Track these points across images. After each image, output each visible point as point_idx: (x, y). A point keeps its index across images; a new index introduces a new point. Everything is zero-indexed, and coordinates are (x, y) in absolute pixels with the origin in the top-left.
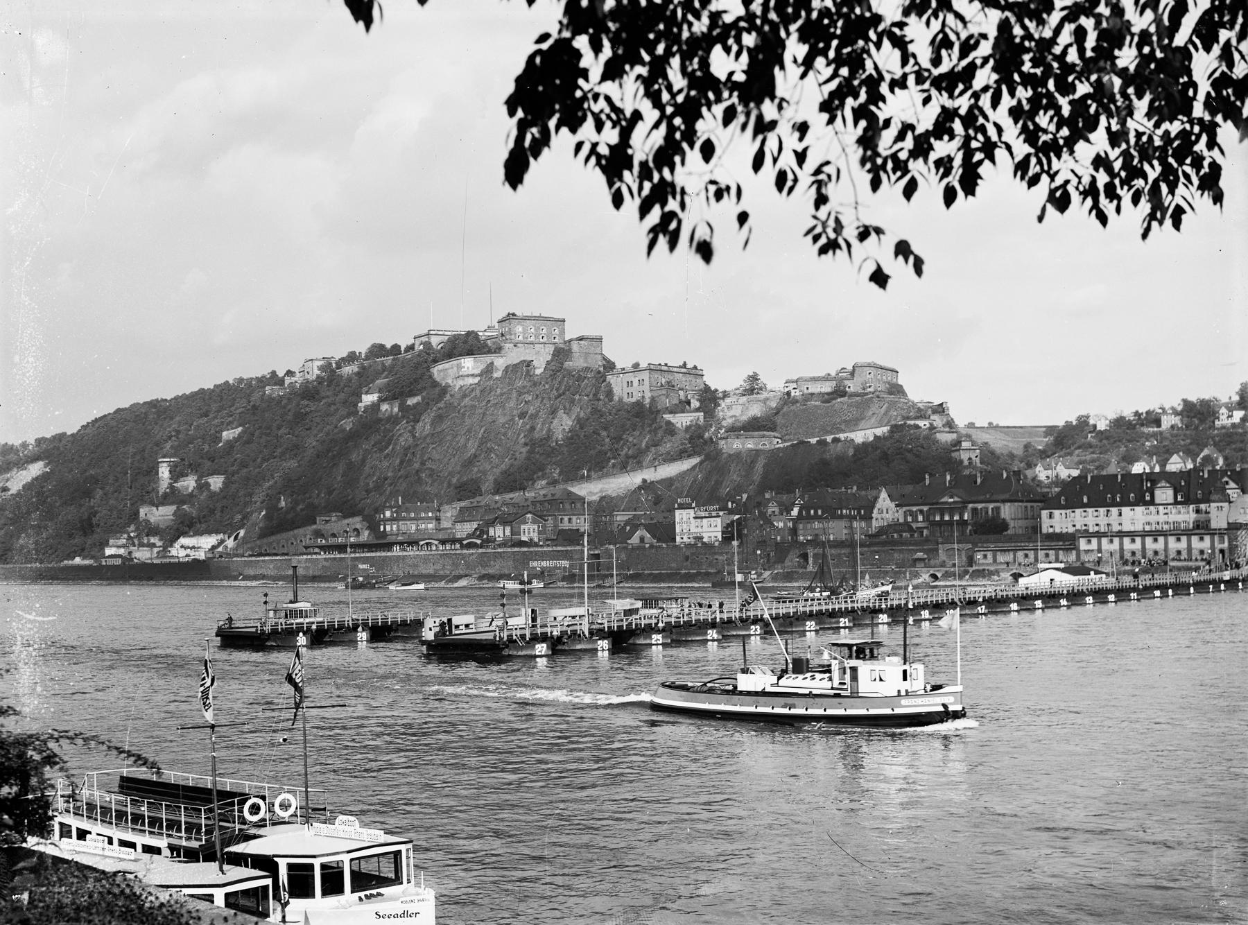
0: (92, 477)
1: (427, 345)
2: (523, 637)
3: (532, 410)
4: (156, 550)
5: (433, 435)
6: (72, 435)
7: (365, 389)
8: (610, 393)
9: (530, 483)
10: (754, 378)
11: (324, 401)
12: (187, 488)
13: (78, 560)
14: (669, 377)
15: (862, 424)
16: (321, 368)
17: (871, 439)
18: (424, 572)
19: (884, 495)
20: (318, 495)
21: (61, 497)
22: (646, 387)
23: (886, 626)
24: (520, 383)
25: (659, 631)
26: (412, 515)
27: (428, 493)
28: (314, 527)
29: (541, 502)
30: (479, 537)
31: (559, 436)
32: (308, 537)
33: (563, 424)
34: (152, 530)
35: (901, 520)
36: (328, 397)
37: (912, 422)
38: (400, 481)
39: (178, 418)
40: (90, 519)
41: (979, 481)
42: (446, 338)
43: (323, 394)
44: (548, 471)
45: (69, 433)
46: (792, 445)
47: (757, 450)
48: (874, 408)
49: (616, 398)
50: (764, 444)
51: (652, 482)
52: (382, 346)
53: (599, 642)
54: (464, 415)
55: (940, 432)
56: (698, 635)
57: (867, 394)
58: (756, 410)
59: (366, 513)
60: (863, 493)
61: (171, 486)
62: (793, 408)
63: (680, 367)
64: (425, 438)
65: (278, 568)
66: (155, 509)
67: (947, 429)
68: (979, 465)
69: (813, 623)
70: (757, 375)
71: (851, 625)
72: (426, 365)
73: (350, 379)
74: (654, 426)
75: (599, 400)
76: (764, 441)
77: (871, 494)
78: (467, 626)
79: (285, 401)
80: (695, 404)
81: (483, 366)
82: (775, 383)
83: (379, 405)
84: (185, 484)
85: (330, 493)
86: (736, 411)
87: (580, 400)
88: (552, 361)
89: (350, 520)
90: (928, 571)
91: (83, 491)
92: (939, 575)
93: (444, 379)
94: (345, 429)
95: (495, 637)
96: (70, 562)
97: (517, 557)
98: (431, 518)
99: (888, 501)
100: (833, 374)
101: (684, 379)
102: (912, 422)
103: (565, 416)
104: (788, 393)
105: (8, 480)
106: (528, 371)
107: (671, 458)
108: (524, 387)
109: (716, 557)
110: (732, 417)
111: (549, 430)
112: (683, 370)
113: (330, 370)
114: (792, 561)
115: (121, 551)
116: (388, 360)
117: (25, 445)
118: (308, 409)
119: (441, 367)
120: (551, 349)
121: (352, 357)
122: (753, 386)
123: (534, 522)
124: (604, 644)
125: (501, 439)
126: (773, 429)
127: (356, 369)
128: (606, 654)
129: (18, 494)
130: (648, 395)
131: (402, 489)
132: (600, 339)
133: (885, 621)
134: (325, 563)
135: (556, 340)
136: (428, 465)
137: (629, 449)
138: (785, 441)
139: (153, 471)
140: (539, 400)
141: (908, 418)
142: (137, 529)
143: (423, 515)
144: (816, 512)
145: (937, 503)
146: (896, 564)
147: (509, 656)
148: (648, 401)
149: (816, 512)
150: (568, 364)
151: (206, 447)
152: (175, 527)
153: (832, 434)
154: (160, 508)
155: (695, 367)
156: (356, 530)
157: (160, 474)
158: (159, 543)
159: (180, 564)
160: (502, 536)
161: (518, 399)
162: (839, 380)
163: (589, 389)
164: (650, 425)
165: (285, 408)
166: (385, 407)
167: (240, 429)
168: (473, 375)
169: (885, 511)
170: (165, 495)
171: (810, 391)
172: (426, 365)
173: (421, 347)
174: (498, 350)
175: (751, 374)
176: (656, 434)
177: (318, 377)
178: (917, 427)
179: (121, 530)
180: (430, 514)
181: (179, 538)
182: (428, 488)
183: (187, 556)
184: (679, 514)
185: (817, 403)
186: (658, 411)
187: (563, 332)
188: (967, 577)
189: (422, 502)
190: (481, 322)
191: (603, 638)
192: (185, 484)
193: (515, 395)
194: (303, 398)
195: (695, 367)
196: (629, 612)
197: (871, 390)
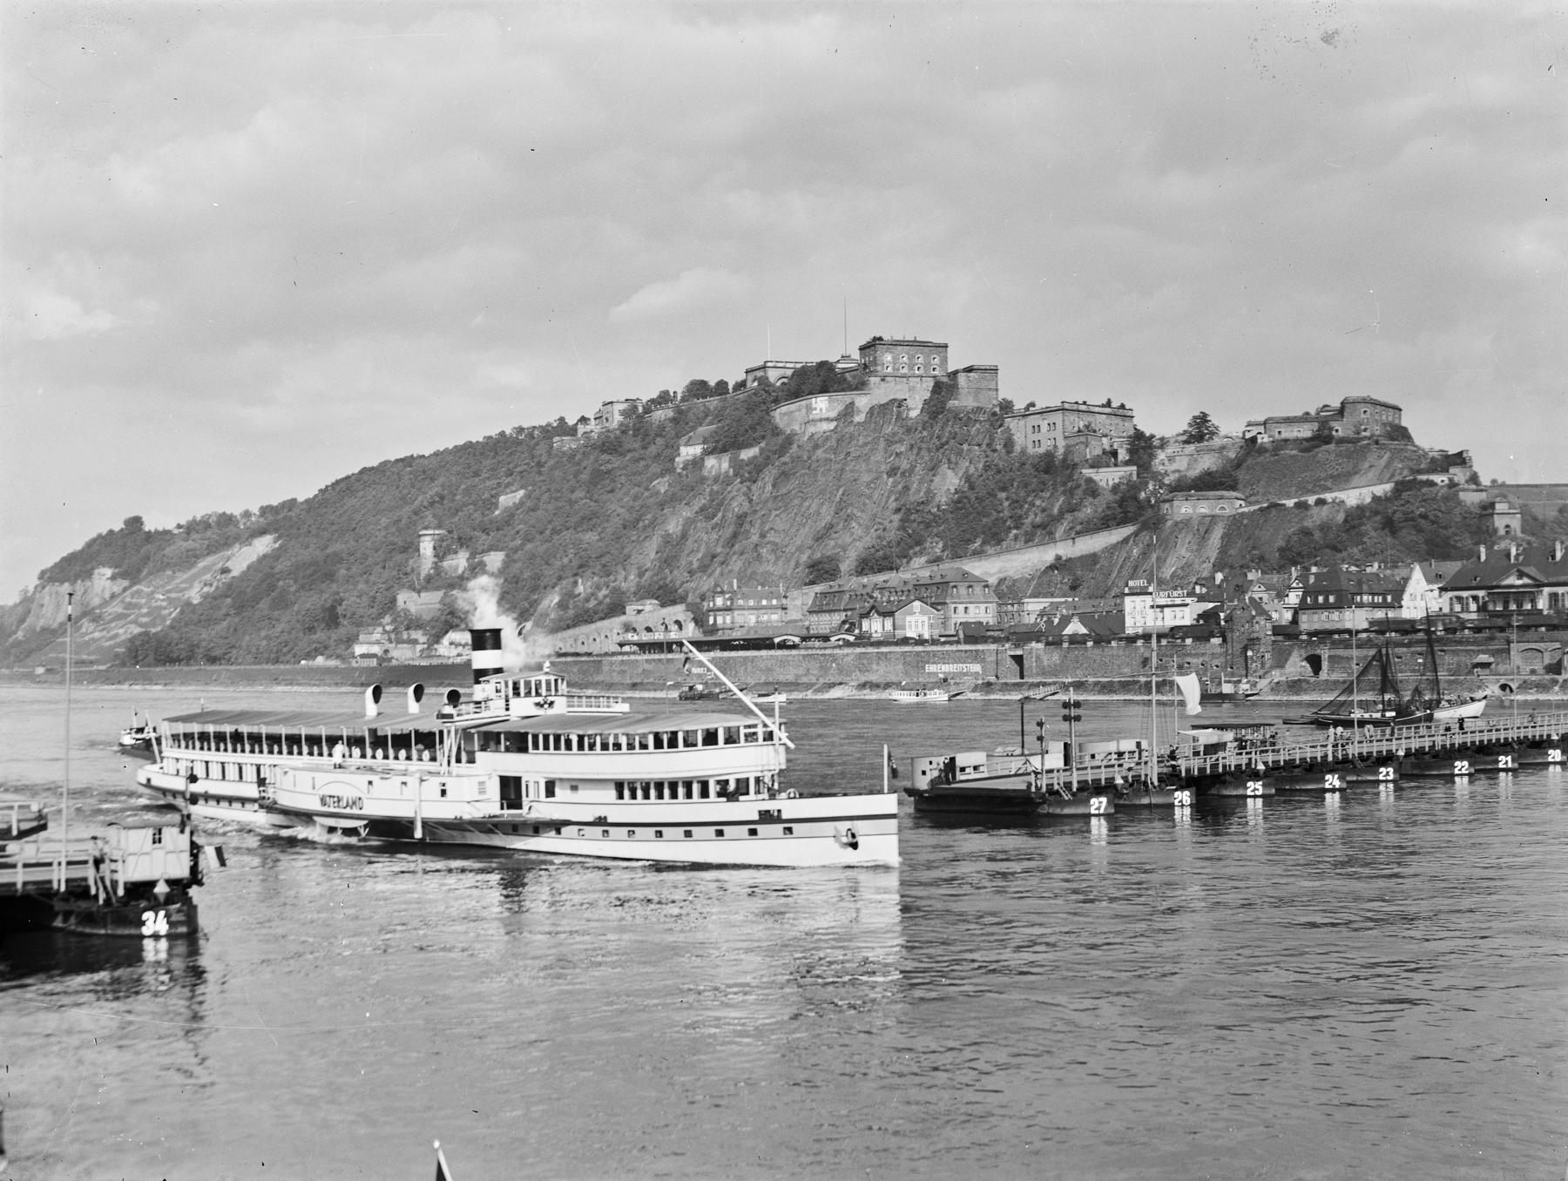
0: (336, 554)
1: (763, 381)
2: (1068, 785)
3: (905, 465)
4: (419, 647)
5: (775, 498)
6: (307, 501)
7: (685, 439)
8: (1009, 444)
9: (905, 561)
10: (1201, 421)
11: (629, 456)
12: (456, 568)
13: (320, 660)
14: (1088, 418)
15: (1356, 480)
16: (623, 413)
17: (1368, 500)
18: (782, 678)
19: (1417, 575)
20: (626, 579)
21: (296, 581)
22: (1058, 433)
23: (1558, 768)
24: (888, 429)
25: (1255, 776)
26: (751, 603)
27: (770, 574)
28: (623, 618)
29: (926, 586)
30: (849, 631)
31: (943, 499)
32: (615, 631)
33: (949, 482)
34: (414, 623)
35: (1446, 610)
36: (634, 450)
37: (1424, 477)
38: (735, 558)
39: (441, 480)
40: (333, 608)
41: (1559, 555)
42: (789, 373)
43: (627, 446)
44: (927, 545)
45: (301, 499)
46: (1261, 510)
47: (1213, 516)
48: (1371, 458)
49: (1017, 448)
50: (1223, 508)
51: (1069, 560)
52: (703, 383)
53: (1177, 794)
54: (816, 472)
55: (1464, 490)
56: (1309, 781)
57: (1363, 439)
58: (1208, 463)
59: (689, 599)
60: (1388, 572)
61: (436, 566)
62: (1261, 459)
63: (1103, 406)
64: (766, 502)
65: (584, 673)
66: (415, 595)
67: (1474, 487)
68: (1519, 534)
69: (1466, 763)
70: (1205, 415)
71: (1516, 765)
72: (764, 407)
73: (662, 427)
74: (1069, 484)
75: (995, 451)
76: (1222, 503)
77: (1399, 573)
78: (975, 768)
79: (578, 457)
80: (1123, 455)
81: (840, 408)
82: (1231, 426)
83: (703, 460)
84: (454, 562)
85: (641, 575)
86: (1181, 464)
87: (969, 450)
88: (931, 399)
89: (670, 609)
90: (1498, 681)
91: (320, 573)
92: (1514, 686)
93: (788, 425)
94: (658, 493)
95: (1030, 785)
96: (311, 663)
97: (908, 659)
98: (776, 608)
99: (1424, 585)
100: (1313, 413)
101: (1108, 422)
102: (1424, 477)
103: (950, 473)
104: (1254, 439)
105: (229, 559)
106: (899, 415)
107: (1090, 528)
108: (894, 434)
109: (1189, 660)
110: (1174, 472)
111: (929, 491)
112: (1107, 410)
113: (637, 415)
114: (1295, 665)
115: (376, 649)
116: (713, 402)
117: (247, 514)
118: (609, 466)
119: (784, 409)
120: (930, 383)
121: (664, 398)
122: (1200, 430)
123: (922, 612)
124: (1184, 797)
125: (865, 504)
126: (1233, 488)
127: (670, 414)
128: (1187, 811)
129: (245, 575)
130: (1061, 444)
131: (737, 568)
132: (995, 370)
133: (1558, 759)
134: (647, 666)
135: (936, 373)
136: (771, 537)
137: (1036, 515)
138: (1251, 504)
139: (411, 548)
140: (915, 451)
141: (1420, 472)
142: (394, 621)
143: (764, 602)
144: (1326, 599)
145: (1498, 587)
146: (1449, 670)
147: (1049, 815)
148: (1061, 451)
149: (1326, 599)
150: (952, 403)
151: (477, 515)
152: (443, 618)
153: (1314, 493)
154: (423, 594)
155: (1122, 406)
156: (678, 623)
157: (422, 551)
158: (422, 639)
159: (453, 665)
160: (880, 630)
161: (886, 451)
162: (1324, 424)
163: (981, 436)
164: (1064, 484)
165: (578, 464)
166: (711, 462)
167: (522, 493)
168: (827, 419)
169: (1419, 597)
170: (429, 579)
171: (1284, 436)
172: (764, 407)
173: (756, 384)
174: (861, 386)
175: (1197, 414)
176: (1072, 495)
177: (621, 424)
178: (1432, 484)
179: (375, 621)
180: (774, 602)
181: (447, 632)
182: (770, 568)
183: (459, 655)
184: (1130, 603)
185: (1294, 452)
186: (1075, 466)
187: (944, 361)
188: (1557, 688)
189: (763, 585)
190: (840, 349)
191: (1182, 788)
192: (454, 562)
193: (882, 444)
194: (603, 451)
195: (1122, 406)
196: (1212, 749)
197: (1367, 434)
